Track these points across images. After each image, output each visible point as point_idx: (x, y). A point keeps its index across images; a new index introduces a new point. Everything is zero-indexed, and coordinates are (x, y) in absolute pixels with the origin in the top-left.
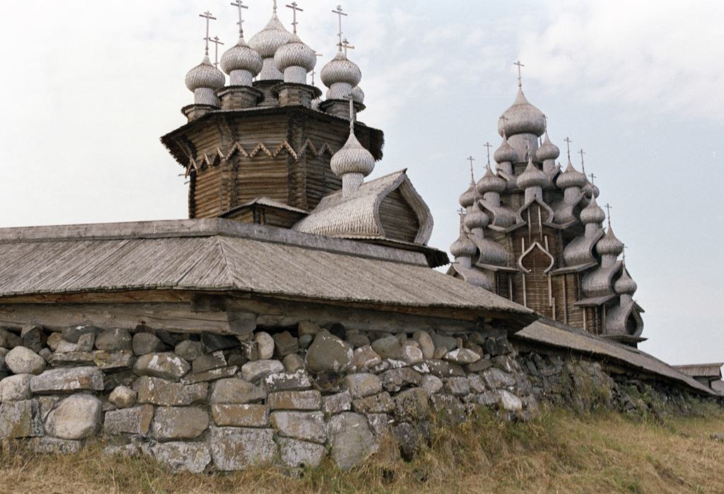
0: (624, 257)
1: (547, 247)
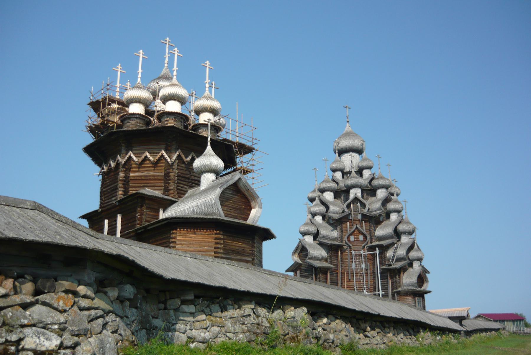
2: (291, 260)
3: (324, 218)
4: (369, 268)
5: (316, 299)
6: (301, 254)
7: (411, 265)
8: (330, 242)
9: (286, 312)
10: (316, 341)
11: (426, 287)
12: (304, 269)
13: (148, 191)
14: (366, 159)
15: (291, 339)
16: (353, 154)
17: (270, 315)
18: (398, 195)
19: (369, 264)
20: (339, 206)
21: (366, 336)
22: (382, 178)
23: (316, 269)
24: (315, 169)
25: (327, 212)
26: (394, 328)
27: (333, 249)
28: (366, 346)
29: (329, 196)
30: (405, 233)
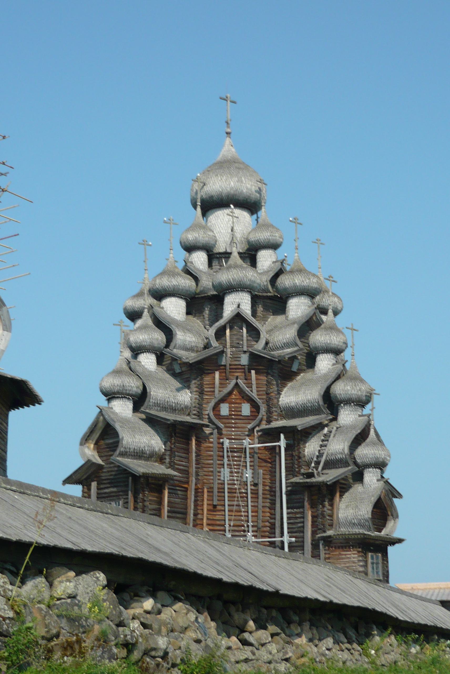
0: (372, 410)
1: (254, 387)
2: (77, 455)
3: (160, 359)
4: (261, 481)
5: (130, 552)
6: (102, 442)
7: (358, 477)
8: (171, 417)
9: (56, 582)
10: (124, 653)
11: (393, 529)
12: (108, 478)
13: (171, 416)
14: (267, 226)
15: (65, 649)
16: (238, 212)
17: (15, 588)
18: (336, 313)
19: (261, 471)
20: (198, 334)
21: (245, 643)
22: (300, 271)
23: (136, 478)
24: (144, 243)
25: (167, 346)
26: (312, 625)
27: (179, 433)
28: (243, 667)
29: (174, 308)
30: (348, 402)
